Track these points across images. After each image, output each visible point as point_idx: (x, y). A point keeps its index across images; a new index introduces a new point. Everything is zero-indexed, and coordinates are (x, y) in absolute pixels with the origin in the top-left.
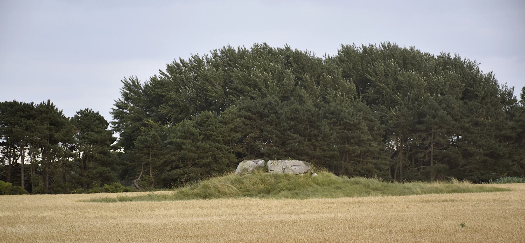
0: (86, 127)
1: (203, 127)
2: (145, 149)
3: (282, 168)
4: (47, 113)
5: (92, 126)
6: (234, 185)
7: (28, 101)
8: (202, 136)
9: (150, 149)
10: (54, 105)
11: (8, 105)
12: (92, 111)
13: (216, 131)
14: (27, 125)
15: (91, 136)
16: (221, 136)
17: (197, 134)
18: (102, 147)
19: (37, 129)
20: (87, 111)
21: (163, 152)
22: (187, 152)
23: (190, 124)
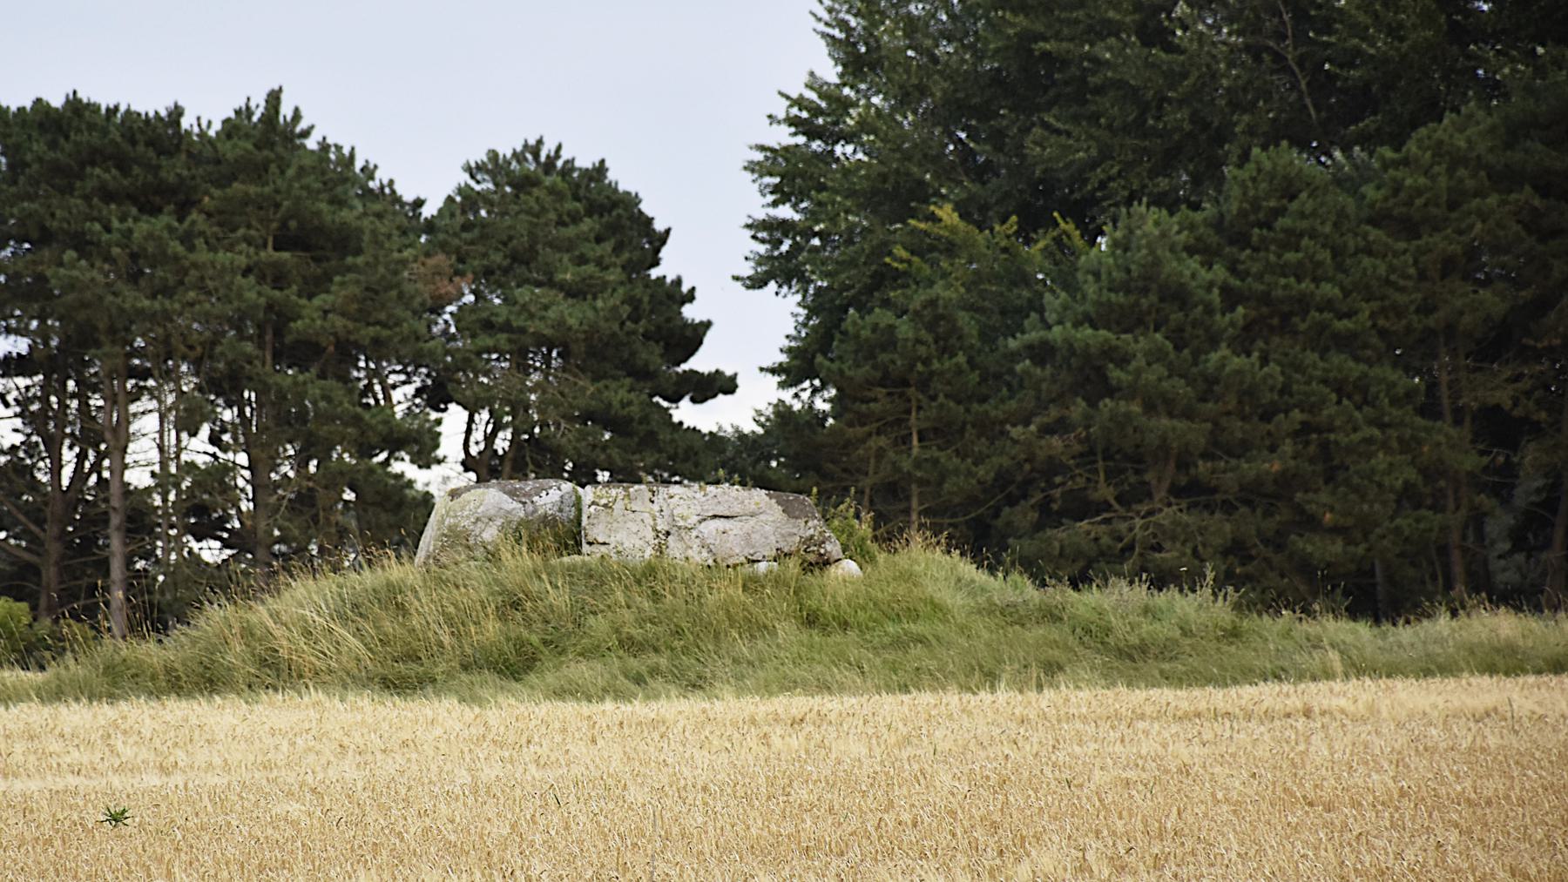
0: (515, 258)
1: (1256, 249)
2: (880, 392)
3: (655, 530)
4: (258, 171)
5: (545, 254)
6: (352, 627)
7: (149, 102)
8: (1240, 310)
9: (911, 391)
10: (302, 125)
11: (41, 118)
12: (566, 155)
13: (1340, 276)
14: (135, 249)
15: (532, 316)
16: (1366, 309)
17: (1208, 297)
18: (601, 385)
19: (193, 272)
20: (536, 155)
21: (993, 413)
22: (1136, 408)
23: (1164, 235)
